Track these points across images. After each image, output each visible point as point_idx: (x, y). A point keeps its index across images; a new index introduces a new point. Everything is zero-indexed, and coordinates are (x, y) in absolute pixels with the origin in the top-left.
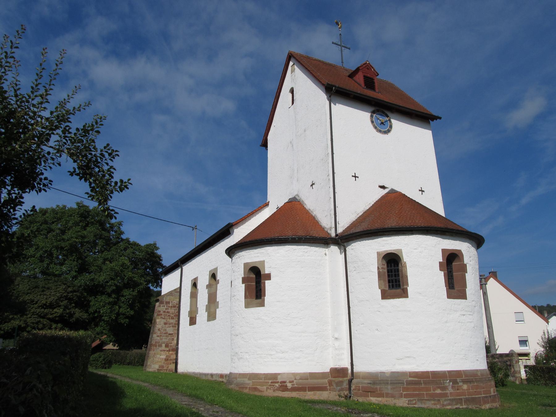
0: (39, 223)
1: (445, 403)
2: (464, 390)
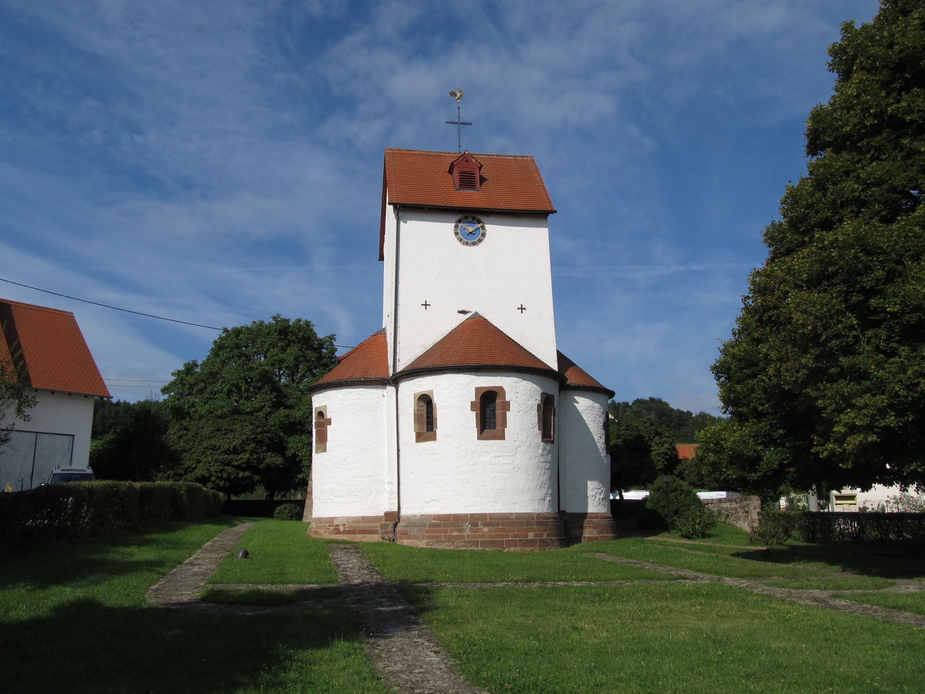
0: (229, 348)
1: (459, 544)
2: (484, 532)
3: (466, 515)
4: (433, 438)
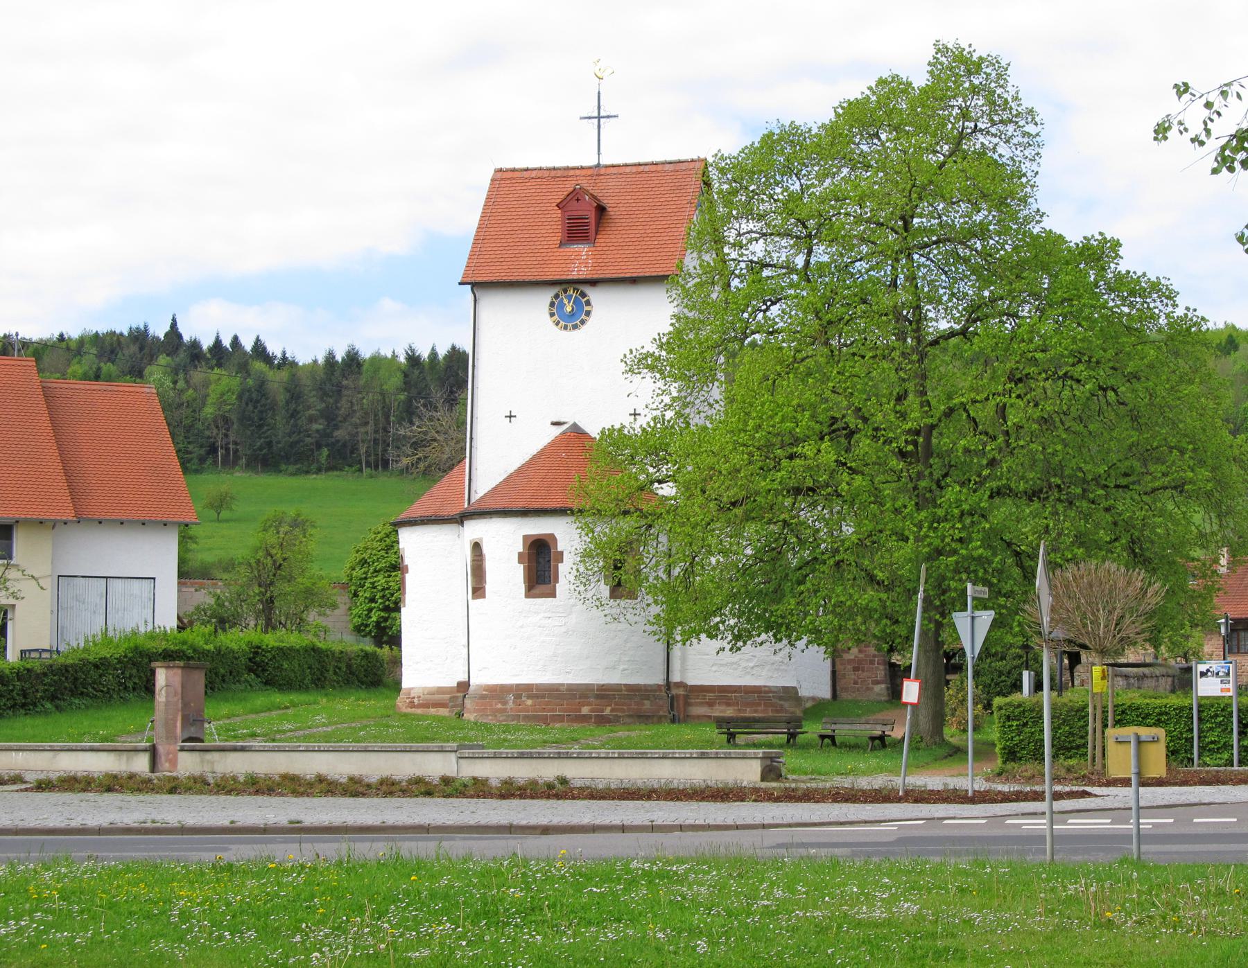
3: (511, 686)
4: (483, 596)
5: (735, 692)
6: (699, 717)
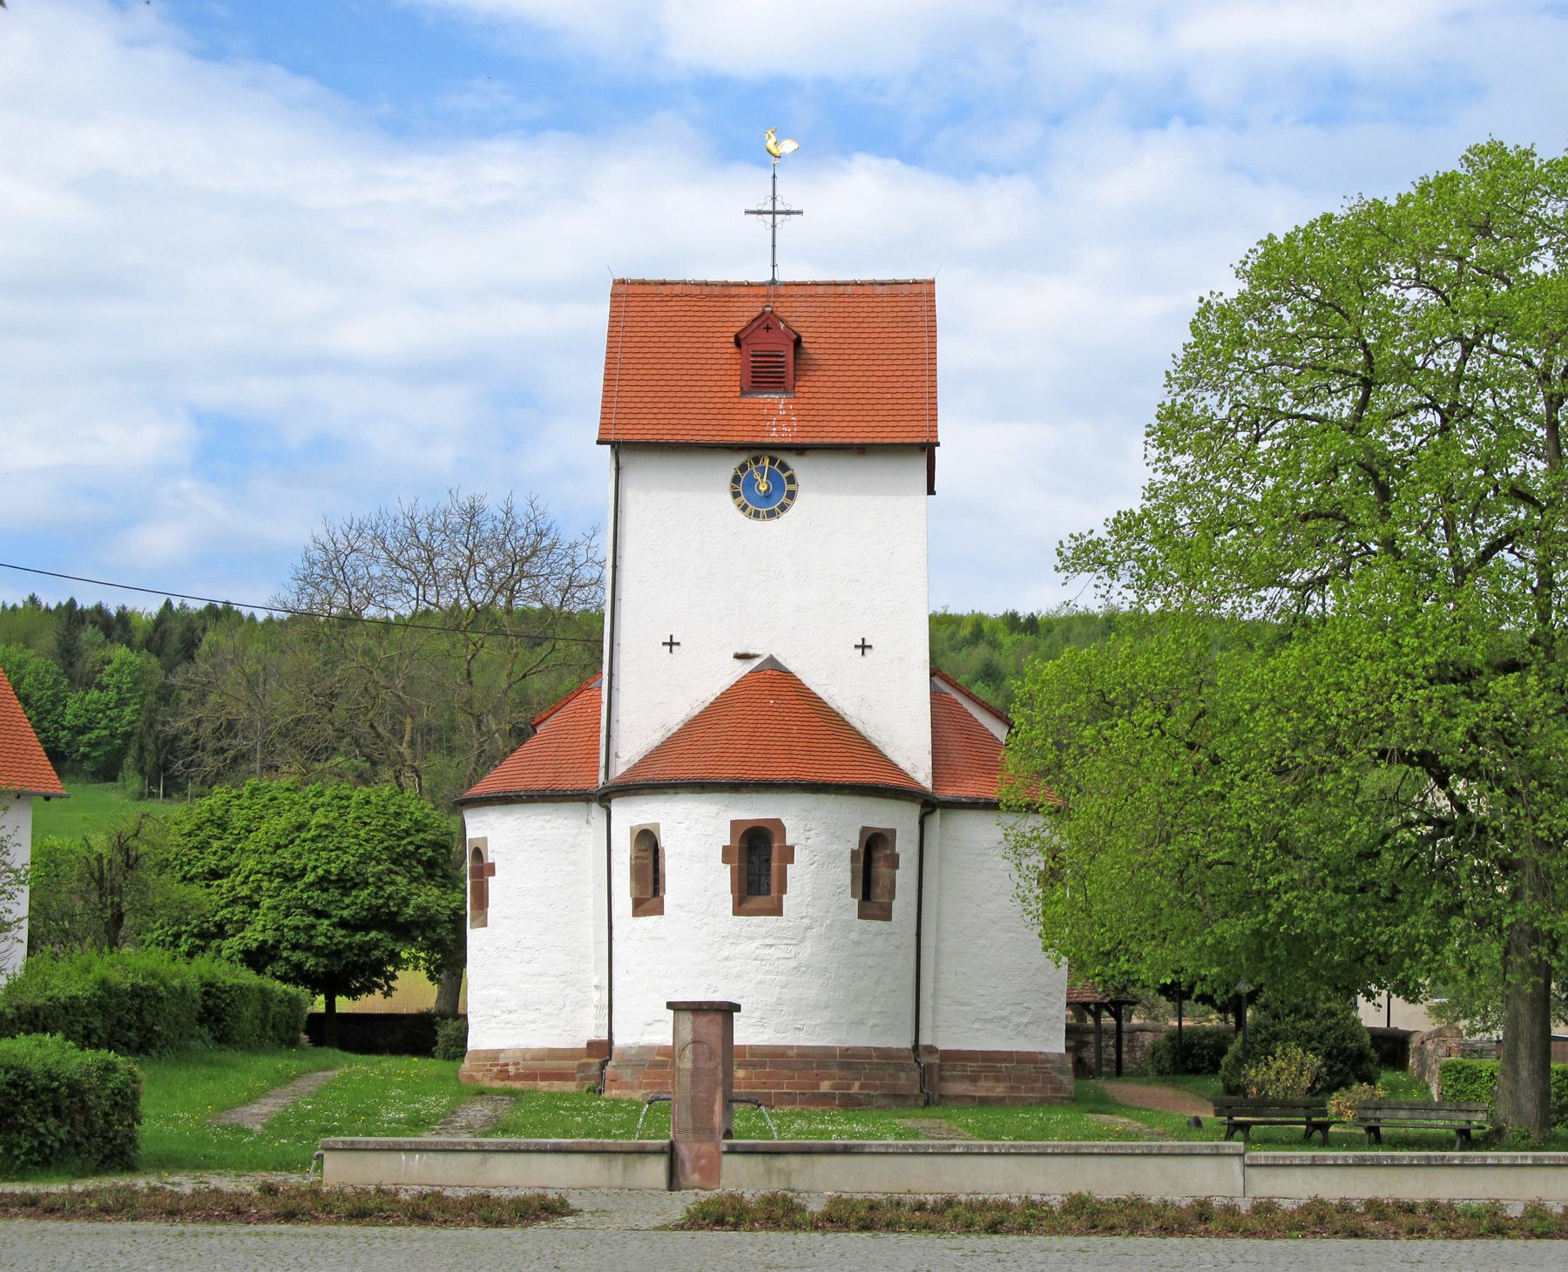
4: (659, 910)
5: (1005, 1060)
6: (959, 1099)
